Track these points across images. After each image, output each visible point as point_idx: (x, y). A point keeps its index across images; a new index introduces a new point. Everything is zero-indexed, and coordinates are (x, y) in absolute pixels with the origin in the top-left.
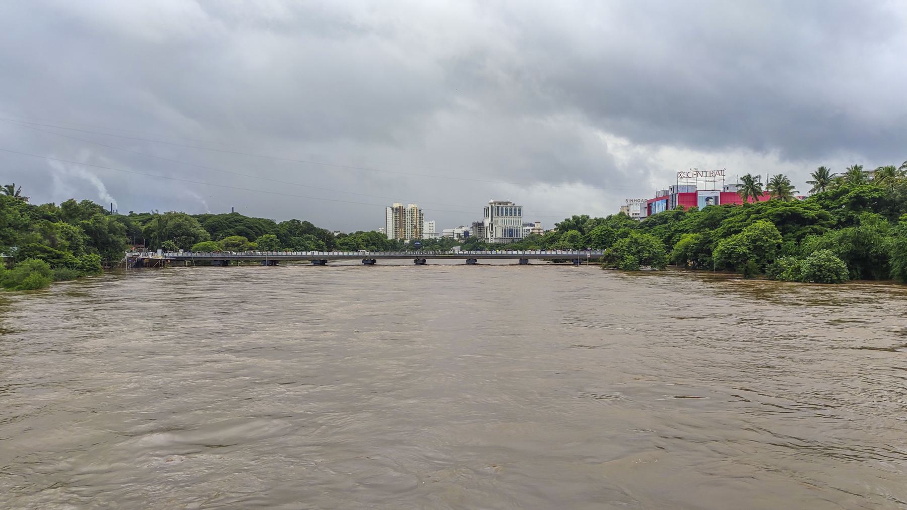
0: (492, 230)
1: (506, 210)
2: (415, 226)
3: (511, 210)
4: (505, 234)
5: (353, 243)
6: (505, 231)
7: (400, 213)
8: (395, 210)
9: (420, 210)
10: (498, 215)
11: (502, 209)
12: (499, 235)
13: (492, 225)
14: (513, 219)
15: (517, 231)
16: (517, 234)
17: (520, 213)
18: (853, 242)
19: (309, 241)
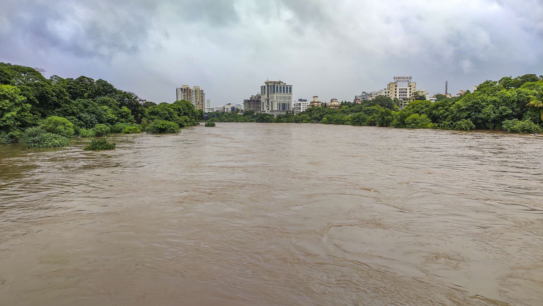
0: (268, 104)
1: (281, 88)
2: (198, 103)
3: (284, 88)
4: (279, 107)
5: (165, 112)
6: (279, 105)
7: (187, 93)
8: (183, 90)
9: (202, 91)
10: (274, 92)
11: (277, 87)
12: (275, 108)
13: (268, 100)
14: (285, 95)
15: (288, 105)
16: (288, 108)
17: (290, 91)
18: (107, 120)
19: (105, 107)
